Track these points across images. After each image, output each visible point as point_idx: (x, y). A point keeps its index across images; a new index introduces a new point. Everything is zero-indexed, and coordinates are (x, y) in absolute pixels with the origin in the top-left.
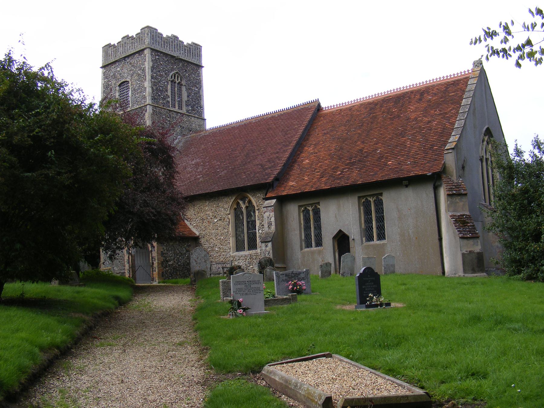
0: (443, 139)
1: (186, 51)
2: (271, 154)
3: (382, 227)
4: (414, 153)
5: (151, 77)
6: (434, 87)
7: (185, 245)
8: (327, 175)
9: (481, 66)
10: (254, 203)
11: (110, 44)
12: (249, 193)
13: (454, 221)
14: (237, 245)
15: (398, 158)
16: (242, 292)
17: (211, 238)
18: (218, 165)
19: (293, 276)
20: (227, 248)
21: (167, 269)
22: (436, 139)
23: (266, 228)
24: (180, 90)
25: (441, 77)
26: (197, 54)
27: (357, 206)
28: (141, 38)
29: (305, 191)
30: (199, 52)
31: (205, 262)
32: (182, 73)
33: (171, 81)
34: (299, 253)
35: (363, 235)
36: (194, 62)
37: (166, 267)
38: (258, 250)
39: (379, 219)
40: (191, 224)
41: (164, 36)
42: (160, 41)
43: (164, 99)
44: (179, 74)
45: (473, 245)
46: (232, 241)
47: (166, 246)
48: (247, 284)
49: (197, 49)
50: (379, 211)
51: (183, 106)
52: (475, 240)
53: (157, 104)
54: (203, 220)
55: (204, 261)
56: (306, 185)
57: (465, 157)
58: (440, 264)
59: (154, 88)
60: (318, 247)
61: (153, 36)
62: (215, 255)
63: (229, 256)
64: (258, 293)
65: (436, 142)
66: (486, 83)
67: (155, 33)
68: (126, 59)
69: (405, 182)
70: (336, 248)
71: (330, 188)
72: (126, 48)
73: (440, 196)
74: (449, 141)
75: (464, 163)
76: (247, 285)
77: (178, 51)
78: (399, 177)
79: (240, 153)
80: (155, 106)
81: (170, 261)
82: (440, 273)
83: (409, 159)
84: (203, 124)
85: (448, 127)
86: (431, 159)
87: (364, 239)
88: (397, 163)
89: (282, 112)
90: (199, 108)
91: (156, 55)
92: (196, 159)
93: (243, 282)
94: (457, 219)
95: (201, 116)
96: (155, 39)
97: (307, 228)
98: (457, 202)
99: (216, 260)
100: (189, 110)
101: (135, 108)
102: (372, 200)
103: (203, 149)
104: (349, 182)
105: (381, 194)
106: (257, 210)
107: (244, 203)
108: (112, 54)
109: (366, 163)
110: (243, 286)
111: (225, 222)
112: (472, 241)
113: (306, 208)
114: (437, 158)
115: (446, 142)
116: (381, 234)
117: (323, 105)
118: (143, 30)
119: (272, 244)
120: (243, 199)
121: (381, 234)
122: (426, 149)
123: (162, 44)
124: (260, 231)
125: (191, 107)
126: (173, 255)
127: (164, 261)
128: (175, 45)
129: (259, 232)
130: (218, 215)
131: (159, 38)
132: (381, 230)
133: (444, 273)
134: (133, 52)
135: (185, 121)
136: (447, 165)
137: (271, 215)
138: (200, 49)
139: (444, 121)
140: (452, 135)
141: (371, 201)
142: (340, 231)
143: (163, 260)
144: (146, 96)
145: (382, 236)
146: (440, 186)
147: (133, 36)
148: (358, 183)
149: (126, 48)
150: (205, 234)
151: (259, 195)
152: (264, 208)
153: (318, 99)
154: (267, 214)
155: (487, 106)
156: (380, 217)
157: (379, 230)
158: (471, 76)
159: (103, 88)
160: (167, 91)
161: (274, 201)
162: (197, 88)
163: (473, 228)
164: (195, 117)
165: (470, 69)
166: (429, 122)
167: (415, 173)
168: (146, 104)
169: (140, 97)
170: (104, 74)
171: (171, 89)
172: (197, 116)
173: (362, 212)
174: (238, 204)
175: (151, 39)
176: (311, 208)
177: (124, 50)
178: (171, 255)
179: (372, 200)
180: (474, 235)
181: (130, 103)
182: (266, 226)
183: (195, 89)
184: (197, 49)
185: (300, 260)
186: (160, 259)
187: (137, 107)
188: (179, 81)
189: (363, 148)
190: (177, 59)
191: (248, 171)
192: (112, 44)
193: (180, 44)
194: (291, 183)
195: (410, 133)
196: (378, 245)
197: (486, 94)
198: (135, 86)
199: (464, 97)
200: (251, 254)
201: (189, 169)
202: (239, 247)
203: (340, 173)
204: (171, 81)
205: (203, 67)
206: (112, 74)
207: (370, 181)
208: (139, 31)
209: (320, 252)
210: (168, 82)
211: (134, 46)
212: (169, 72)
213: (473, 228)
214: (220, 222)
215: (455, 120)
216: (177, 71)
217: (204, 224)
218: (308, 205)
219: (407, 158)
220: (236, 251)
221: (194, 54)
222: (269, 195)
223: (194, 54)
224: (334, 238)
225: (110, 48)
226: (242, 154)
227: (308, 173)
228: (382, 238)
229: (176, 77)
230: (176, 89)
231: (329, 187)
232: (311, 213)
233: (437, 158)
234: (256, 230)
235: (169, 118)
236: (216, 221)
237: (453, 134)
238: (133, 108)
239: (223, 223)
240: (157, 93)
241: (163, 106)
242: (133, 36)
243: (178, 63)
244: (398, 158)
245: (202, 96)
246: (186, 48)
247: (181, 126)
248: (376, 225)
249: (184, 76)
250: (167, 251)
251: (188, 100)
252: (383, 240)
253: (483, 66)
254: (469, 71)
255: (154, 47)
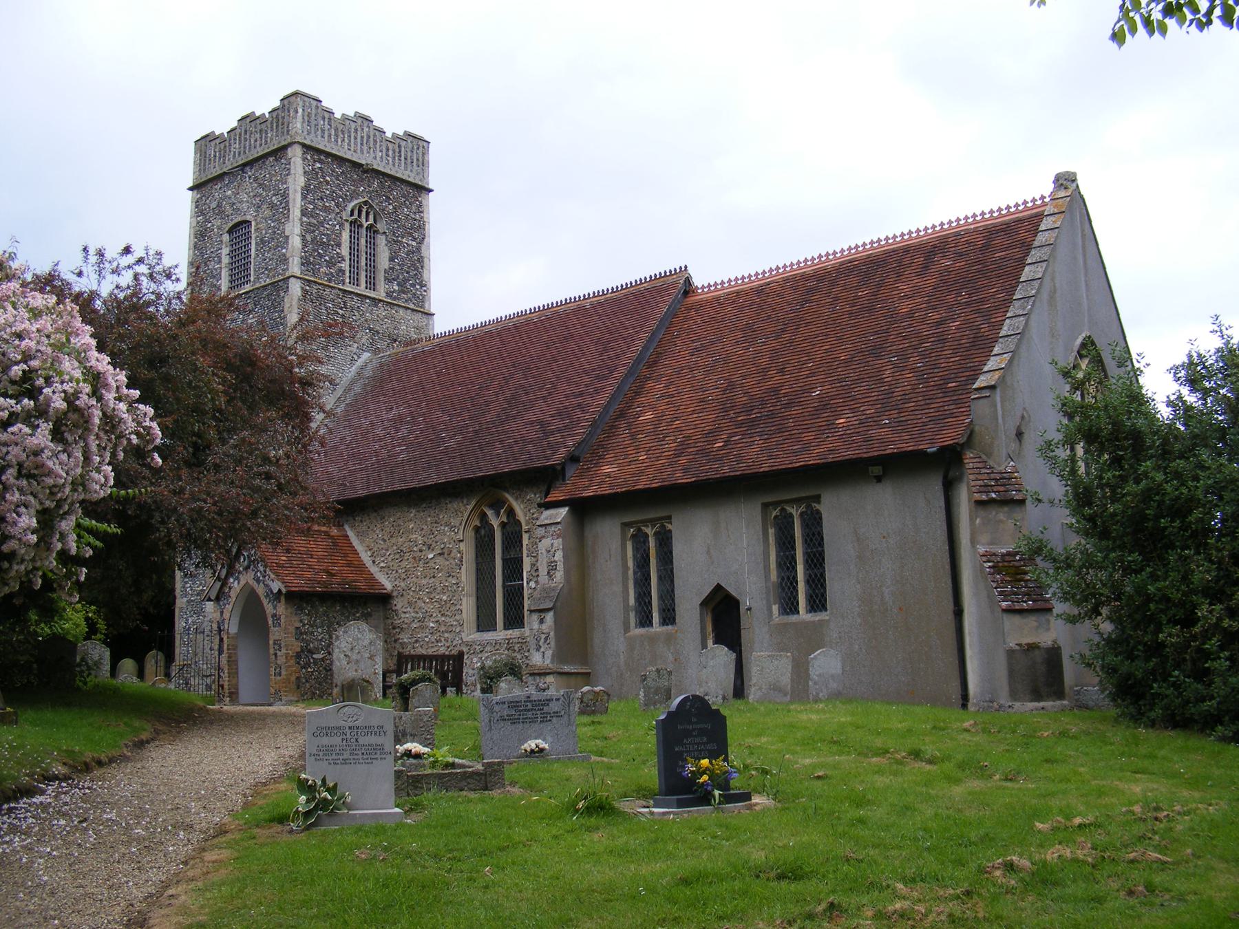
0: (972, 365)
1: (390, 153)
2: (567, 396)
3: (819, 580)
4: (899, 398)
5: (302, 211)
6: (959, 237)
7: (358, 612)
8: (692, 450)
9: (1074, 185)
10: (521, 516)
11: (213, 132)
12: (508, 492)
13: (990, 567)
14: (478, 617)
15: (862, 409)
16: (334, 756)
17: (419, 599)
18: (444, 422)
19: (530, 707)
20: (455, 623)
21: (309, 670)
22: (955, 363)
23: (544, 578)
24: (372, 244)
25: (978, 213)
26: (418, 160)
27: (759, 527)
28: (281, 120)
29: (636, 488)
30: (423, 154)
31: (370, 658)
32: (377, 204)
33: (351, 223)
34: (622, 639)
35: (772, 599)
36: (410, 180)
37: (307, 665)
38: (526, 631)
39: (812, 561)
40: (374, 562)
41: (335, 116)
42: (327, 127)
43: (331, 264)
44: (371, 206)
45: (1038, 627)
46: (468, 607)
47: (308, 615)
48: (348, 734)
49: (418, 149)
50: (811, 540)
51: (377, 282)
52: (1043, 618)
53: (314, 275)
54: (402, 554)
55: (367, 655)
56: (641, 473)
57: (1024, 409)
58: (956, 673)
59: (309, 238)
60: (667, 625)
61: (308, 116)
62: (427, 639)
63: (460, 642)
64: (377, 759)
65: (956, 371)
66: (1088, 231)
67: (313, 109)
68: (248, 168)
69: (877, 470)
70: (709, 628)
71: (695, 481)
72: (247, 143)
73: (959, 505)
74: (986, 369)
75: (1020, 423)
76: (349, 736)
77: (368, 152)
78: (859, 456)
79: (497, 394)
80: (309, 281)
81: (317, 650)
82: (956, 695)
83: (887, 413)
84: (426, 325)
85: (987, 334)
86: (940, 413)
87: (775, 608)
88: (857, 422)
89: (603, 297)
90: (418, 287)
91: (315, 161)
92: (397, 408)
93: (337, 728)
94: (998, 562)
95: (421, 307)
96: (314, 122)
97: (643, 582)
98: (1001, 521)
99: (429, 650)
100: (393, 292)
101: (263, 284)
102: (795, 511)
103: (415, 384)
104: (741, 468)
105: (817, 499)
106: (526, 532)
107: (498, 514)
108: (215, 156)
109: (786, 421)
110: (337, 740)
111: (452, 561)
112: (1034, 618)
113: (639, 530)
114: (955, 411)
115: (978, 372)
116: (817, 596)
117: (698, 281)
118: (286, 102)
119: (555, 613)
120: (497, 505)
121: (817, 596)
122: (928, 389)
123: (330, 136)
124: (532, 584)
125: (398, 285)
126: (327, 637)
127: (302, 651)
128: (362, 137)
129: (528, 587)
130: (436, 542)
131: (324, 121)
132: (816, 585)
133: (965, 697)
134: (261, 151)
135: (382, 317)
136: (977, 428)
137: (555, 545)
138: (423, 147)
139: (978, 319)
140: (993, 353)
141: (794, 514)
142: (718, 588)
143: (299, 650)
144: (288, 255)
145: (818, 602)
146: (959, 479)
147: (264, 114)
148: (762, 470)
149: (247, 143)
150: (406, 588)
151: (531, 496)
152: (540, 529)
153: (686, 267)
154: (546, 543)
155: (1087, 285)
156: (815, 555)
157: (811, 586)
158: (1048, 210)
159: (192, 236)
160: (339, 245)
161: (564, 511)
162: (414, 239)
163: (1037, 587)
164: (407, 308)
165: (1047, 194)
166: (940, 323)
167: (898, 446)
168: (287, 275)
169: (275, 257)
170: (197, 203)
171: (351, 242)
172: (412, 306)
173: (771, 541)
174: (483, 516)
175: (303, 122)
176: (652, 529)
177: (242, 149)
178: (320, 638)
179: (795, 511)
180: (1040, 605)
181: (252, 273)
182: (543, 571)
183: (410, 242)
184: (418, 149)
185: (622, 657)
186: (292, 646)
187: (268, 281)
188: (371, 221)
189: (782, 385)
190: (366, 171)
191: (509, 438)
192: (217, 133)
193: (375, 136)
194: (607, 469)
195: (894, 347)
196: (806, 624)
197: (1084, 256)
198: (264, 232)
199: (1029, 261)
200: (509, 639)
201: (380, 432)
202: (485, 622)
203: (721, 444)
204: (351, 223)
205: (431, 191)
206: (214, 205)
207: (790, 466)
208: (277, 104)
209: (669, 639)
210: (341, 225)
211: (266, 138)
212: (346, 200)
213: (1037, 587)
214: (440, 560)
215: (1004, 318)
216: (366, 199)
217: (405, 563)
218: (645, 522)
219: (883, 409)
220: (475, 630)
221: (409, 160)
222: (555, 496)
223: (409, 160)
224: (704, 604)
225: (213, 143)
226: (502, 397)
227: (648, 445)
228: (818, 606)
229: (364, 214)
230: (363, 241)
231: (693, 479)
232: (652, 543)
233: (955, 411)
234: (523, 580)
235: (341, 308)
236: (431, 556)
237: (996, 350)
238: (258, 285)
239: (448, 563)
240: (315, 250)
241: (330, 280)
242: (264, 114)
243: (369, 181)
244: (862, 409)
245: (425, 260)
246: (390, 146)
247: (371, 329)
248: (805, 574)
249: (383, 210)
250: (311, 626)
251: (390, 268)
252: (821, 611)
253: (1078, 186)
254: (1045, 198)
255: (312, 141)
